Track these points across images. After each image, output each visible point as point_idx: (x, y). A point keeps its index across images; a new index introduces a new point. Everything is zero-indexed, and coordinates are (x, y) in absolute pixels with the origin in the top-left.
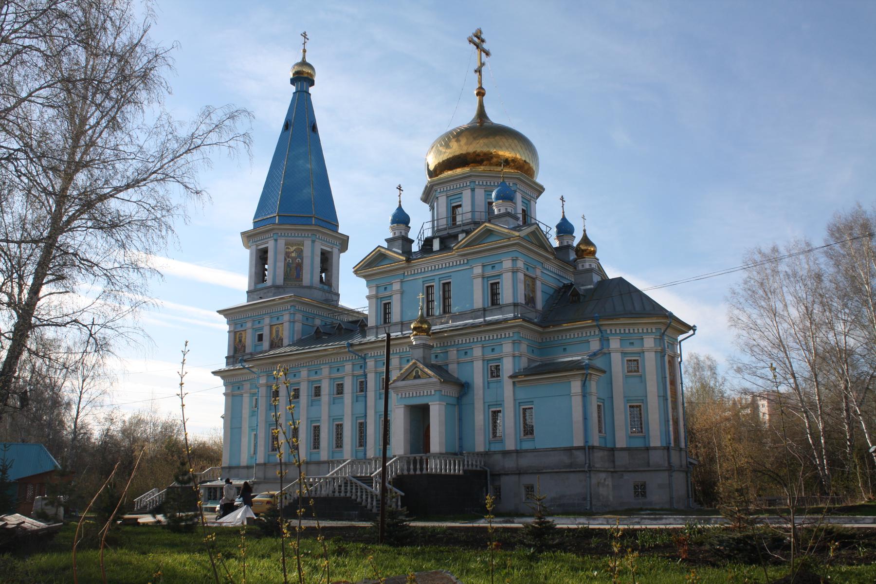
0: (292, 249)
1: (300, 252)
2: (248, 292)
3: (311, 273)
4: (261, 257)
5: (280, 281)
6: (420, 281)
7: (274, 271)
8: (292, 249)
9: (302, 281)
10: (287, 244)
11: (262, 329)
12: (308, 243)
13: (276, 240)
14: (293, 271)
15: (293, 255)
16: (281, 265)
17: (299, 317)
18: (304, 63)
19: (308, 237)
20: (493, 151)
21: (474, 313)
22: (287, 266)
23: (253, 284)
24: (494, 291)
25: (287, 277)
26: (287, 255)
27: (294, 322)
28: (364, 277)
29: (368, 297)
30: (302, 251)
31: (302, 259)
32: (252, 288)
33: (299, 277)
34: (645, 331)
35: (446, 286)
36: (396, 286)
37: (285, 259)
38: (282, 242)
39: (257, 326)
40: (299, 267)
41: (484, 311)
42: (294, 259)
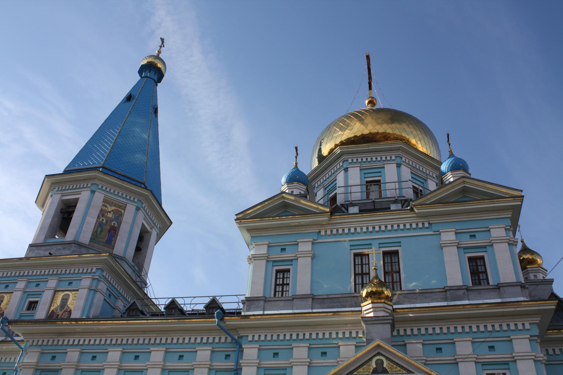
0: (110, 209)
1: (119, 216)
2: (31, 246)
3: (124, 245)
4: (64, 215)
5: (85, 238)
6: (347, 245)
7: (83, 226)
8: (110, 209)
9: (113, 249)
10: (106, 201)
11: (40, 294)
12: (130, 209)
13: (93, 192)
14: (106, 233)
15: (110, 215)
16: (91, 221)
17: (102, 286)
18: (157, 57)
19: (133, 201)
20: (404, 134)
21: (448, 292)
22: (99, 224)
23: (43, 237)
24: (477, 268)
25: (94, 238)
26: (102, 213)
27: (95, 291)
28: (249, 230)
29: (253, 259)
30: (121, 215)
31: (120, 224)
32: (41, 241)
33: (110, 242)
34: (294, 337)
35: (391, 256)
36: (305, 247)
37: (98, 217)
38: (99, 197)
39: (32, 288)
40: (114, 232)
41: (466, 291)
42: (109, 220)
